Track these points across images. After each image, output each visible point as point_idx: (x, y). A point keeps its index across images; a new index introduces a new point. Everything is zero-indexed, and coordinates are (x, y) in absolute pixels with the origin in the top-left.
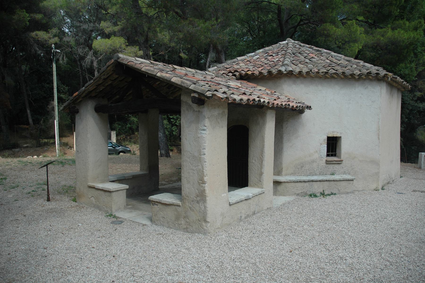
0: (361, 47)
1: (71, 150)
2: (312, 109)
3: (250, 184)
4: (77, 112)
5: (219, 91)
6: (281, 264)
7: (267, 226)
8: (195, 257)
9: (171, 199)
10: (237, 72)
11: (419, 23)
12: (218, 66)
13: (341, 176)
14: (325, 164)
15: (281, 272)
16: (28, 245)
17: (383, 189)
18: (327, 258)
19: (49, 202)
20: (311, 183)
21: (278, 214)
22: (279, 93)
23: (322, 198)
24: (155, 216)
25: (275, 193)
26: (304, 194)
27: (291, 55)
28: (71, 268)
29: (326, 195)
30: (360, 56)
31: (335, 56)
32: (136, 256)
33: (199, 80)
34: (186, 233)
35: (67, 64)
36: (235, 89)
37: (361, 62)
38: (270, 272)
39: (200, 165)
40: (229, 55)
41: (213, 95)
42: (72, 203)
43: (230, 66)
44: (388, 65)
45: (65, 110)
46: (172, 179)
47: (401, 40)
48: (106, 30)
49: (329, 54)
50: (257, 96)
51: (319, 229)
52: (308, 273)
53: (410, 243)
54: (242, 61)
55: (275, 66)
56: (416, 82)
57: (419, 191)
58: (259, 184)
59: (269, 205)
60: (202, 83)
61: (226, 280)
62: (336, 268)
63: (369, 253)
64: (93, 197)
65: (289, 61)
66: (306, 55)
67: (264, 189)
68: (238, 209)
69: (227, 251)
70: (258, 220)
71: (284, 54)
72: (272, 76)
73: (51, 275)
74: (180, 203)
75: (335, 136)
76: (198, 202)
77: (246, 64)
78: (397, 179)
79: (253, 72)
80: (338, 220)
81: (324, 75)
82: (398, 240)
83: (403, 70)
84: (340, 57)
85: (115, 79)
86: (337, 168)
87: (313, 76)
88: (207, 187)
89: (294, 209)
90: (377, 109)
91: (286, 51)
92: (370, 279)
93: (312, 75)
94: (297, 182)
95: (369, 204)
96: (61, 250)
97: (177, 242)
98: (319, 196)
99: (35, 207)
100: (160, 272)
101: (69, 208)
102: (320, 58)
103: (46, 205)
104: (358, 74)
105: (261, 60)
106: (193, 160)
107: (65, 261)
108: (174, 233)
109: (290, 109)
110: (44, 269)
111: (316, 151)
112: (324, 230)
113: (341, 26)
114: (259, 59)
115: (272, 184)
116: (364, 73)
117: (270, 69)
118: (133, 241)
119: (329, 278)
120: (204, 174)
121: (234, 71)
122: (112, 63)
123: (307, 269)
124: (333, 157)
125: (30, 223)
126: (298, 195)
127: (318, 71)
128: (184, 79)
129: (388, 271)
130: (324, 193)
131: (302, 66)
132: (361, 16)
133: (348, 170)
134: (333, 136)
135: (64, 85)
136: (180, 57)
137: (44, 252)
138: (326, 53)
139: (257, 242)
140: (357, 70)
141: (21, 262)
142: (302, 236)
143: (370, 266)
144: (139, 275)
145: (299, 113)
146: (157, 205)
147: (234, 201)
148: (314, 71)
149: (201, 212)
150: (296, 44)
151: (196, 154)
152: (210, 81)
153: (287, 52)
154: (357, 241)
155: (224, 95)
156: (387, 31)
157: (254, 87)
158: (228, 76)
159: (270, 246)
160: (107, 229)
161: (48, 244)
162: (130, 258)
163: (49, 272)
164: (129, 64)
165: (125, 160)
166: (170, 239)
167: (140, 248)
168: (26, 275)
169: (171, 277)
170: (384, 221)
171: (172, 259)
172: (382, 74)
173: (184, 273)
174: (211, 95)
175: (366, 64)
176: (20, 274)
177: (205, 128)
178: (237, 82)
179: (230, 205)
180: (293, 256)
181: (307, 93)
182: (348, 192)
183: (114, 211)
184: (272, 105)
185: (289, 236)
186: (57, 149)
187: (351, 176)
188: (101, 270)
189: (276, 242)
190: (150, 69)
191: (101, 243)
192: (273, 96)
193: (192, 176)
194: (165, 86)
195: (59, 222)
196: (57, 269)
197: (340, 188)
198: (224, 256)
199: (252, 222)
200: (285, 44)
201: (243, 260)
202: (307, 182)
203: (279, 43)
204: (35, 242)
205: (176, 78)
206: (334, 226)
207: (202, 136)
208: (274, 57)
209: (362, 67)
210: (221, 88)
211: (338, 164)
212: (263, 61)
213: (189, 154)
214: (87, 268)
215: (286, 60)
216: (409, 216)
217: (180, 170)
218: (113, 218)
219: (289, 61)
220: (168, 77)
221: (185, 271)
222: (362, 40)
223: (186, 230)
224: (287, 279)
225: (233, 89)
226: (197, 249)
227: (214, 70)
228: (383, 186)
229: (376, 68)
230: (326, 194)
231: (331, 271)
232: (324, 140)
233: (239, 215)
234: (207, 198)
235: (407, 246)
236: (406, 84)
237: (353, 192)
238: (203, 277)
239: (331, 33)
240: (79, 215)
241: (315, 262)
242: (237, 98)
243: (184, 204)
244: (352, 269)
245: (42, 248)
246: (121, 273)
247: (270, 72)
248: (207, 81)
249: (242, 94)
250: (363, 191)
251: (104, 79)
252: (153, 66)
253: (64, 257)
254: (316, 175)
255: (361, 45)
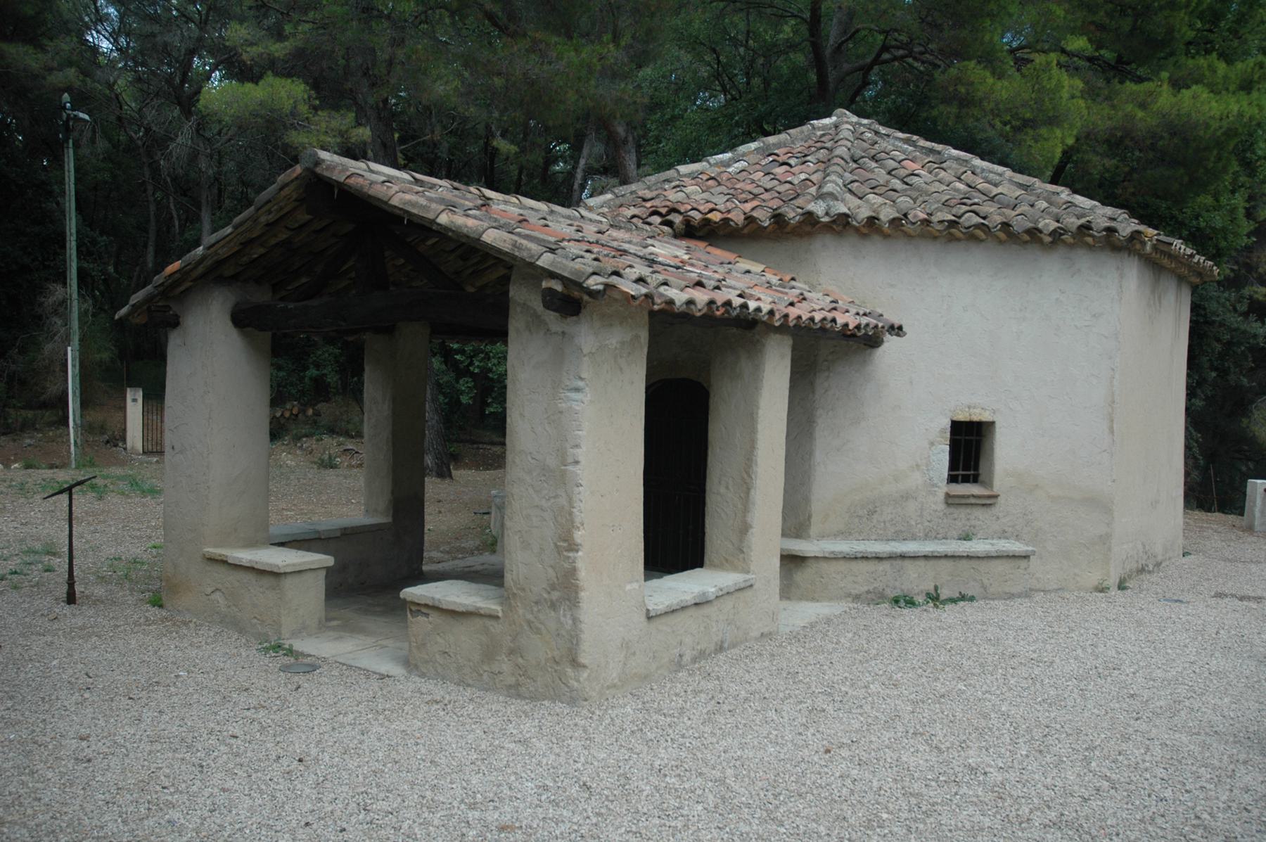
0: (1070, 141)
1: (114, 449)
2: (905, 334)
3: (710, 561)
4: (175, 323)
5: (625, 276)
6: (796, 782)
7: (758, 684)
8: (544, 762)
9: (470, 596)
10: (676, 215)
11: (1257, 68)
12: (617, 191)
13: (992, 545)
14: (942, 506)
15: (795, 801)
16: (26, 729)
17: (1121, 587)
18: (931, 768)
19: (72, 605)
20: (899, 562)
21: (794, 653)
22: (805, 283)
23: (931, 609)
24: (418, 648)
25: (787, 591)
26: (876, 598)
27: (847, 162)
28: (172, 790)
29: (944, 602)
30: (1070, 168)
31: (983, 170)
32: (366, 760)
33: (563, 240)
34: (514, 701)
35: (104, 160)
36: (672, 269)
37: (1062, 192)
38: (765, 802)
39: (564, 495)
40: (651, 153)
41: (607, 286)
42: (147, 611)
43: (654, 194)
44: (1158, 197)
45: (136, 315)
46: (463, 545)
47: (1201, 122)
48: (246, 52)
49: (965, 164)
50: (739, 292)
51: (914, 695)
52: (873, 805)
53: (1177, 735)
54: (694, 176)
55: (795, 198)
56: (1252, 252)
57: (1233, 596)
58: (738, 558)
59: (767, 626)
60: (574, 249)
61: (638, 821)
62: (956, 794)
63: (1055, 758)
64: (220, 590)
65: (837, 185)
66: (892, 164)
67: (753, 576)
68: (673, 632)
69: (639, 748)
70: (731, 667)
71: (825, 160)
72: (786, 230)
73: (115, 809)
74: (499, 608)
75: (975, 418)
76: (553, 606)
77: (704, 188)
78: (1173, 561)
79: (725, 215)
80: (974, 671)
81: (945, 230)
82: (1144, 727)
83: (1205, 214)
84: (1000, 175)
85: (301, 227)
86: (981, 518)
87: (913, 233)
88: (582, 561)
89: (842, 640)
90: (1106, 337)
91: (830, 150)
92: (1048, 822)
93: (908, 228)
94: (856, 558)
95: (1072, 630)
96: (135, 742)
97: (489, 724)
98: (923, 604)
99: (27, 620)
100: (444, 800)
101: (140, 625)
102: (936, 176)
103: (65, 615)
104: (1052, 228)
105: (751, 177)
106: (543, 478)
107: (153, 772)
108: (478, 700)
109: (838, 332)
110: (90, 793)
111: (917, 465)
112: (929, 698)
113: (1012, 71)
114: (744, 173)
115: (776, 562)
116: (1069, 226)
117: (779, 208)
118: (354, 719)
119: (932, 820)
120: (573, 522)
121: (666, 209)
122: (296, 178)
123: (871, 797)
124: (968, 485)
125: (19, 668)
126: (857, 598)
127: (926, 217)
128: (519, 235)
129: (1101, 803)
130: (938, 595)
131: (880, 200)
132: (1081, 35)
133: (1013, 527)
134: (968, 420)
135: (92, 230)
136: (493, 153)
137: (83, 750)
138: (957, 159)
139: (729, 726)
140: (1048, 217)
141: (13, 775)
142: (862, 711)
143: (1053, 790)
144: (384, 807)
145: (865, 345)
146: (427, 615)
147: (661, 608)
148: (915, 216)
149: (564, 636)
150: (862, 129)
151: (552, 462)
152: (597, 242)
153: (833, 155)
154: (1024, 726)
155: (639, 287)
156: (1158, 90)
157: (727, 261)
158: (650, 224)
159: (765, 738)
160: (269, 685)
161: (90, 727)
162: (352, 764)
163: (108, 803)
164: (352, 181)
165: (304, 484)
166: (468, 715)
167: (379, 740)
168: (38, 808)
169: (477, 814)
170: (1111, 676)
171: (477, 768)
172: (1124, 230)
173: (515, 804)
174: (601, 287)
175: (1078, 197)
176: (17, 807)
177: (581, 384)
178: (676, 245)
179: (649, 618)
180: (832, 762)
181: (892, 286)
182: (1013, 595)
183: (287, 636)
184: (782, 320)
185: (824, 711)
186: (72, 441)
187: (1022, 546)
188: (265, 796)
189: (784, 726)
190: (417, 203)
191: (256, 726)
192: (786, 293)
193: (537, 527)
194: (453, 251)
195: (114, 667)
196: (132, 795)
197: (987, 581)
198: (632, 762)
199: (713, 671)
200: (830, 129)
201: (686, 770)
202: (885, 558)
203: (810, 124)
204: (48, 720)
205: (496, 230)
206: (961, 686)
207: (571, 407)
208: (792, 170)
209: (1065, 209)
210: (631, 266)
211: (983, 505)
212: (759, 180)
213: (530, 459)
214: (224, 790)
215: (831, 182)
216: (1187, 665)
217: (486, 517)
218: (285, 655)
219: (837, 185)
220: (471, 228)
221: (519, 796)
222: (1074, 119)
223: (514, 691)
224: (814, 820)
225: (665, 270)
226: (551, 741)
227: (605, 203)
228: (1125, 578)
229: (1109, 211)
230: (942, 597)
231: (939, 801)
232: (942, 431)
233: (676, 651)
234: (582, 594)
235: (1168, 742)
236: (1202, 261)
237: (1028, 594)
238: (571, 814)
239: (980, 94)
240: (176, 647)
241: (896, 780)
242: (679, 296)
243: (511, 611)
244: (1001, 798)
245: (73, 738)
246: (327, 805)
247: (778, 218)
248: (588, 242)
249: (691, 285)
250: (1060, 593)
251: (267, 225)
252: (421, 189)
253: (146, 763)
254: (914, 538)
255: (1071, 135)
